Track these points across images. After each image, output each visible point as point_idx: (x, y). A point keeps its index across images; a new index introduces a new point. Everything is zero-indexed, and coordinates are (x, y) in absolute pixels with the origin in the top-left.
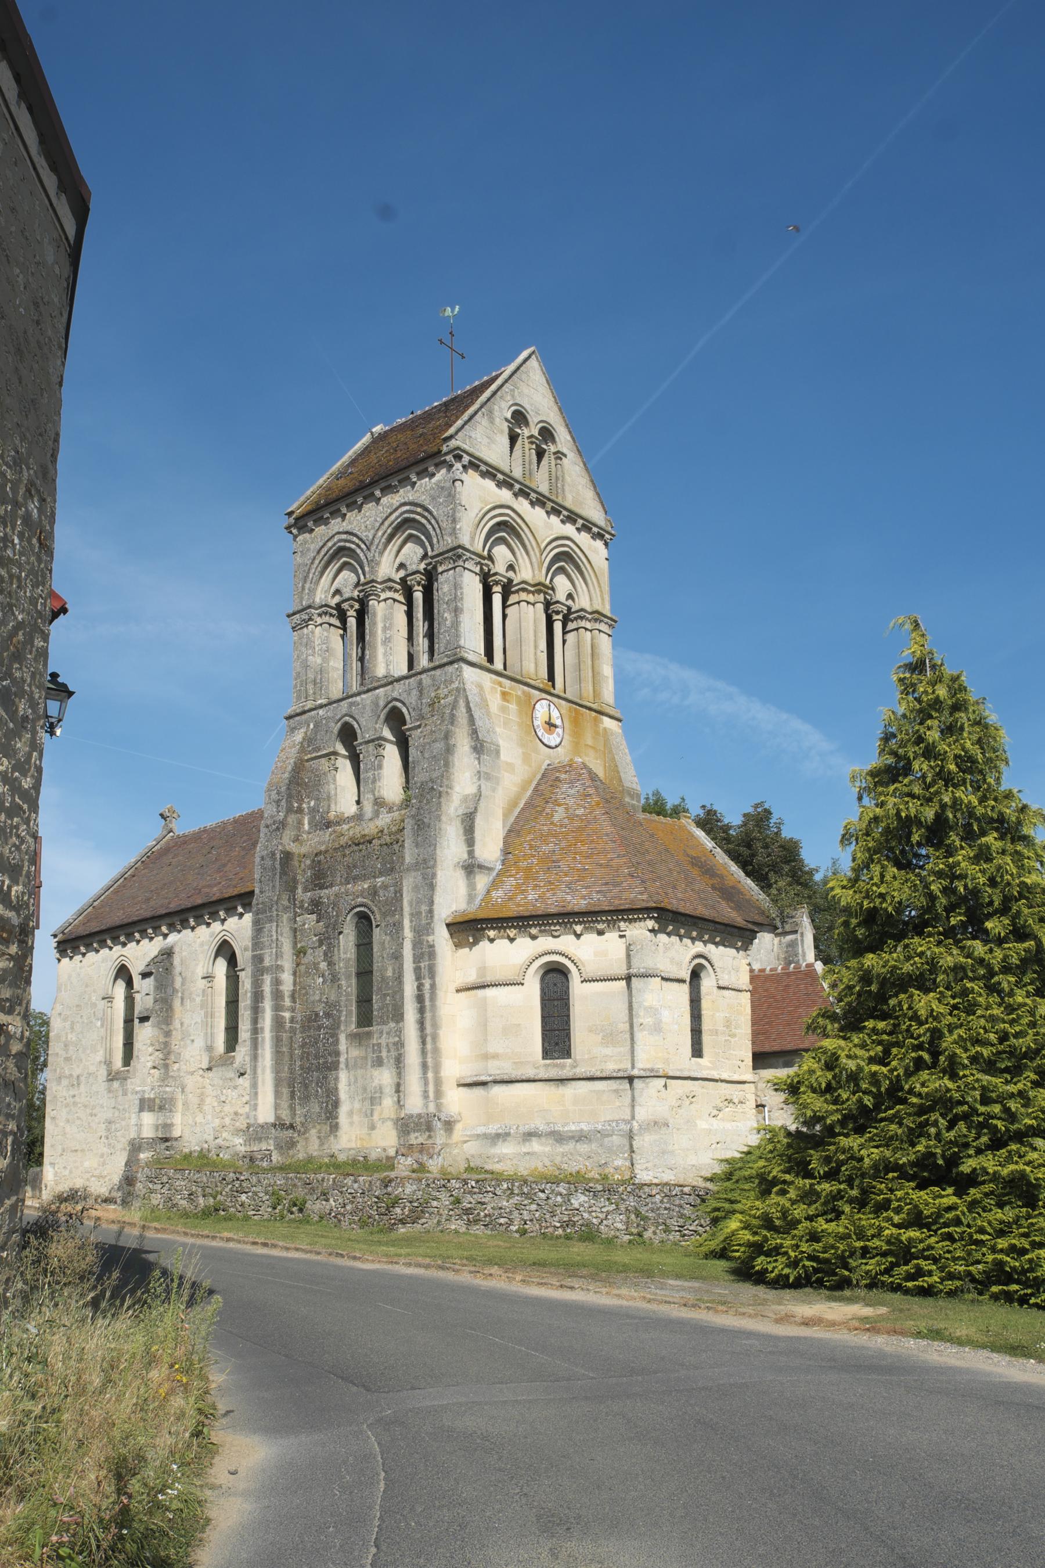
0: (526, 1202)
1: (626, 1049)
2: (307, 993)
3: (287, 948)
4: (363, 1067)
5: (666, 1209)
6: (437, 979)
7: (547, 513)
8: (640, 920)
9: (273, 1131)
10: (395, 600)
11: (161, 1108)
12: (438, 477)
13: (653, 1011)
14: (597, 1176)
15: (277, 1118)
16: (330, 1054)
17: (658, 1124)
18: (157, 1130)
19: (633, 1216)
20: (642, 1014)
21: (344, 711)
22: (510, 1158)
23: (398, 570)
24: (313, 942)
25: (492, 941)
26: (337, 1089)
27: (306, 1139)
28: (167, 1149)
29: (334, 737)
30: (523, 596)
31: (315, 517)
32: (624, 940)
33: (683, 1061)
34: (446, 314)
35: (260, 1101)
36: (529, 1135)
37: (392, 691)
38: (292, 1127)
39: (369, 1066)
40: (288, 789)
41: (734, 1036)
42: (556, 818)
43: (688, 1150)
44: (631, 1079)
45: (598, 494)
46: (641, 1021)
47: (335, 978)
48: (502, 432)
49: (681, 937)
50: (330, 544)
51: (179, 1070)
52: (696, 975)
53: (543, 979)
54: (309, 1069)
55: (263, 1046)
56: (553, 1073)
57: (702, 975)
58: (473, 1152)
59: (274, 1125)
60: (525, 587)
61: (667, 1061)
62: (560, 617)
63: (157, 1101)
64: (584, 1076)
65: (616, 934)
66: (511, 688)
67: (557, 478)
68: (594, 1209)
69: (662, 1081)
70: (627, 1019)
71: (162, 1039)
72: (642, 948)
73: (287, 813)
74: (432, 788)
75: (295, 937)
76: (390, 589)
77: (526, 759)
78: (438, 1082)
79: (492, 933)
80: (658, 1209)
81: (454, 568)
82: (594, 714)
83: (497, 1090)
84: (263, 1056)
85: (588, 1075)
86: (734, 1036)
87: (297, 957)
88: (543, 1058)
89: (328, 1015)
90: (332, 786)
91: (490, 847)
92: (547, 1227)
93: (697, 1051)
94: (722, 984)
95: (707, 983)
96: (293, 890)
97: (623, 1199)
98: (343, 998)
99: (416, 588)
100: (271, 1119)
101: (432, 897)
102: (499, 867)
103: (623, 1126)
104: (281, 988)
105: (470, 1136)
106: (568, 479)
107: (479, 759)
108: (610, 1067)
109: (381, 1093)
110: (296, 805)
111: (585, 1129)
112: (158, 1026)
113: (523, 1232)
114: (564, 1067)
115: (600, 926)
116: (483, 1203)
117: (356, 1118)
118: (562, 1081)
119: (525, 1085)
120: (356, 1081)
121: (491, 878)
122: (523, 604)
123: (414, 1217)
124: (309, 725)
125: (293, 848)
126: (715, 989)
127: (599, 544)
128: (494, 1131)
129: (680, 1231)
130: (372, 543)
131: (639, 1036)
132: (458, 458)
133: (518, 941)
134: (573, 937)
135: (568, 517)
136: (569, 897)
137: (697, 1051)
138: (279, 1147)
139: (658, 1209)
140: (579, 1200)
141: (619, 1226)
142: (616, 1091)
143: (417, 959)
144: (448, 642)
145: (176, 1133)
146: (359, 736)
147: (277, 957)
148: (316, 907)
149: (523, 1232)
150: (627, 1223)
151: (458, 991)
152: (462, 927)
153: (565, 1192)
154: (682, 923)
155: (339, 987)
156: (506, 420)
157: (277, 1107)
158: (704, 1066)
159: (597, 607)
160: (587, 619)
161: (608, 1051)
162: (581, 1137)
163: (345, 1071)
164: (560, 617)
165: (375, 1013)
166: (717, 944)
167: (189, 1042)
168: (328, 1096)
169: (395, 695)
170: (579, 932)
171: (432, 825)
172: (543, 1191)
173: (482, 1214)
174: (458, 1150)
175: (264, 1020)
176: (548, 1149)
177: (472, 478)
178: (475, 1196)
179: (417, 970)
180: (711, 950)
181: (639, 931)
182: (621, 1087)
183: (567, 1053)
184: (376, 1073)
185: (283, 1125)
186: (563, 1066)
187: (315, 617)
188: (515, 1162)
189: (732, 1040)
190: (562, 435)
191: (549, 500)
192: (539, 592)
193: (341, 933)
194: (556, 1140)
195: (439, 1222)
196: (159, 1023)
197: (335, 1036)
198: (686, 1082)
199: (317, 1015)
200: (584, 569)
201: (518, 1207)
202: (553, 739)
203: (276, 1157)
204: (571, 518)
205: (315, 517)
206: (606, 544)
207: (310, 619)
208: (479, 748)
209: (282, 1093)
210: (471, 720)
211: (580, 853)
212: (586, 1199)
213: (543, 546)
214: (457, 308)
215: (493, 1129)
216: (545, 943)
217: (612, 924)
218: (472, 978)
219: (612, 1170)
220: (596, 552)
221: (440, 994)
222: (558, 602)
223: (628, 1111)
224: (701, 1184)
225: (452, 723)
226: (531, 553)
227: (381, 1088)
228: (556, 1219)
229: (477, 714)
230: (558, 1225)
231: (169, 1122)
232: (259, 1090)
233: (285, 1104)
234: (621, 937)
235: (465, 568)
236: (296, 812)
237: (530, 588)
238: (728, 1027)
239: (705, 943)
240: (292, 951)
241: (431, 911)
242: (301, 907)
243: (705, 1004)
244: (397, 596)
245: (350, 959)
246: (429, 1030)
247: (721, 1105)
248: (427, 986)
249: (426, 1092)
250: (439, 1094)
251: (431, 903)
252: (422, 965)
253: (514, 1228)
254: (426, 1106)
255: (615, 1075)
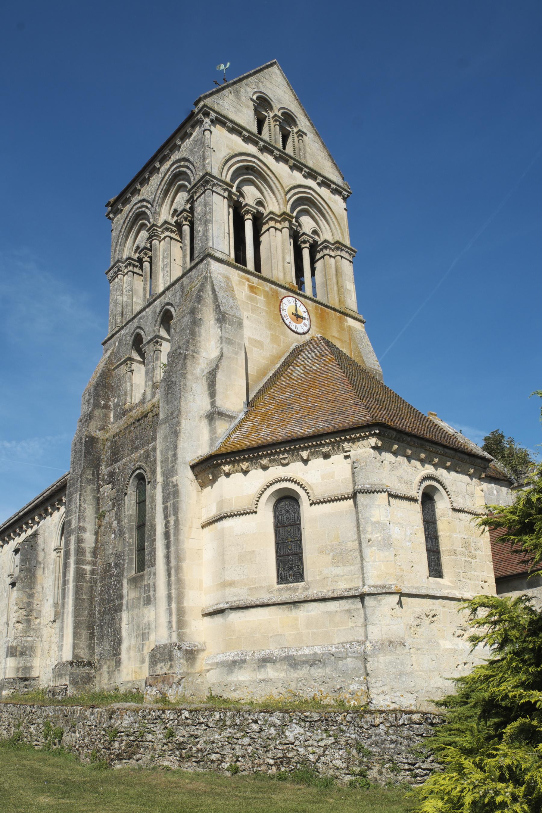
0: (238, 735)
1: (355, 567)
2: (105, 549)
3: (90, 512)
4: (138, 607)
5: (392, 742)
6: (180, 516)
7: (290, 167)
8: (363, 438)
9: (69, 668)
10: (171, 238)
11: (22, 654)
12: (194, 134)
13: (380, 526)
14: (332, 702)
15: (75, 656)
16: (117, 598)
17: (392, 644)
18: (18, 671)
19: (354, 752)
20: (369, 529)
21: (136, 325)
22: (247, 686)
23: (173, 216)
24: (109, 506)
25: (228, 475)
26: (120, 628)
27: (101, 674)
28: (26, 687)
29: (130, 346)
30: (272, 223)
31: (122, 201)
32: (349, 460)
33: (419, 577)
34: (221, 68)
35: (65, 643)
36: (264, 661)
37: (165, 298)
38: (89, 664)
39: (141, 606)
40: (95, 390)
41: (474, 557)
42: (295, 374)
43: (431, 671)
44: (362, 597)
45: (335, 164)
46: (369, 536)
47: (122, 533)
48: (248, 107)
49: (409, 458)
50: (131, 214)
51: (39, 624)
52: (428, 498)
53: (276, 507)
54: (104, 612)
55: (68, 595)
56: (286, 596)
57: (436, 498)
58: (213, 680)
59: (71, 663)
60: (272, 216)
61: (400, 578)
62: (307, 245)
63: (19, 648)
64: (316, 597)
65: (341, 456)
66: (258, 284)
67: (300, 149)
68: (310, 742)
69: (396, 598)
70: (356, 537)
71: (25, 600)
72: (366, 465)
73: (94, 407)
74: (180, 353)
75: (98, 504)
76: (167, 229)
77: (275, 339)
78: (181, 612)
79: (227, 468)
80: (383, 742)
81: (204, 192)
82: (338, 314)
83: (234, 617)
84: (68, 603)
85: (320, 596)
86: (474, 557)
87: (99, 520)
88: (278, 583)
89: (117, 564)
90: (128, 384)
91: (233, 400)
92: (260, 765)
93: (435, 570)
94: (456, 505)
95: (442, 505)
96: (97, 466)
97: (342, 731)
98: (127, 549)
99: (184, 223)
100: (70, 658)
101: (176, 442)
102: (242, 416)
103: (357, 648)
104: (83, 545)
105: (211, 665)
106: (308, 150)
107: (221, 327)
108: (342, 587)
109: (149, 629)
110: (102, 402)
111: (319, 652)
112: (23, 589)
113: (235, 771)
114: (298, 590)
115: (325, 449)
116: (196, 737)
117: (132, 653)
118: (295, 603)
119: (260, 610)
120: (133, 621)
121: (233, 425)
122: (272, 230)
123: (128, 754)
124: (115, 344)
125: (99, 434)
126: (450, 512)
127: (338, 199)
128: (231, 659)
129: (410, 770)
130: (154, 201)
131: (368, 552)
132: (207, 114)
133: (252, 473)
134: (301, 464)
135: (308, 173)
136: (297, 429)
137: (435, 570)
138: (74, 682)
139: (383, 742)
140: (294, 731)
141: (339, 763)
142: (349, 611)
143: (165, 500)
144: (201, 247)
145: (34, 674)
146: (144, 337)
147: (79, 520)
148: (112, 478)
149: (235, 771)
150: (348, 760)
151: (203, 527)
152: (202, 466)
153: (279, 723)
154: (408, 444)
155: (124, 540)
156: (252, 99)
157: (75, 646)
158: (444, 585)
159: (339, 238)
160: (330, 249)
161: (339, 571)
162: (315, 661)
163: (126, 612)
164: (307, 245)
165: (146, 557)
166: (448, 469)
167: (45, 601)
168: (115, 635)
169: (167, 300)
170: (305, 458)
171: (178, 383)
172: (256, 722)
173: (194, 749)
174: (207, 677)
175: (69, 573)
176: (283, 675)
177: (219, 132)
178: (188, 729)
179: (165, 509)
180: (442, 473)
181: (363, 449)
182: (354, 607)
183: (300, 577)
184: (146, 611)
185: (81, 662)
186: (295, 590)
187: (123, 269)
188: (251, 689)
189: (473, 561)
190: (303, 122)
191: (291, 157)
192: (284, 220)
193: (126, 494)
194: (290, 665)
195: (153, 758)
196: (23, 587)
197: (120, 582)
198: (424, 600)
199: (110, 564)
200: (325, 212)
201: (230, 740)
202: (301, 327)
203: (70, 691)
204: (312, 174)
205: (122, 201)
206: (345, 199)
207: (119, 270)
208: (222, 318)
209: (81, 635)
210: (216, 298)
211: (312, 396)
212: (302, 731)
213: (286, 189)
214: (228, 64)
215: (230, 656)
216: (277, 471)
217: (337, 446)
218: (212, 512)
219: (348, 696)
220: (337, 204)
221: (184, 529)
222: (304, 234)
223: (361, 631)
224: (432, 709)
225: (199, 302)
226: (276, 192)
227: (149, 624)
228: (270, 755)
229: (221, 294)
230: (272, 762)
231: (29, 665)
232: (65, 633)
233: (83, 643)
234: (347, 457)
235: (213, 192)
236: (103, 408)
237: (277, 218)
238: (467, 548)
239: (436, 466)
240: (94, 515)
241: (175, 455)
242: (103, 480)
243: (442, 527)
244: (173, 235)
245: (131, 515)
246: (173, 563)
247: (466, 624)
248: (172, 523)
249: (170, 622)
250: (181, 623)
251: (176, 447)
252: (169, 504)
253: (225, 766)
254: (170, 636)
255: (346, 594)
